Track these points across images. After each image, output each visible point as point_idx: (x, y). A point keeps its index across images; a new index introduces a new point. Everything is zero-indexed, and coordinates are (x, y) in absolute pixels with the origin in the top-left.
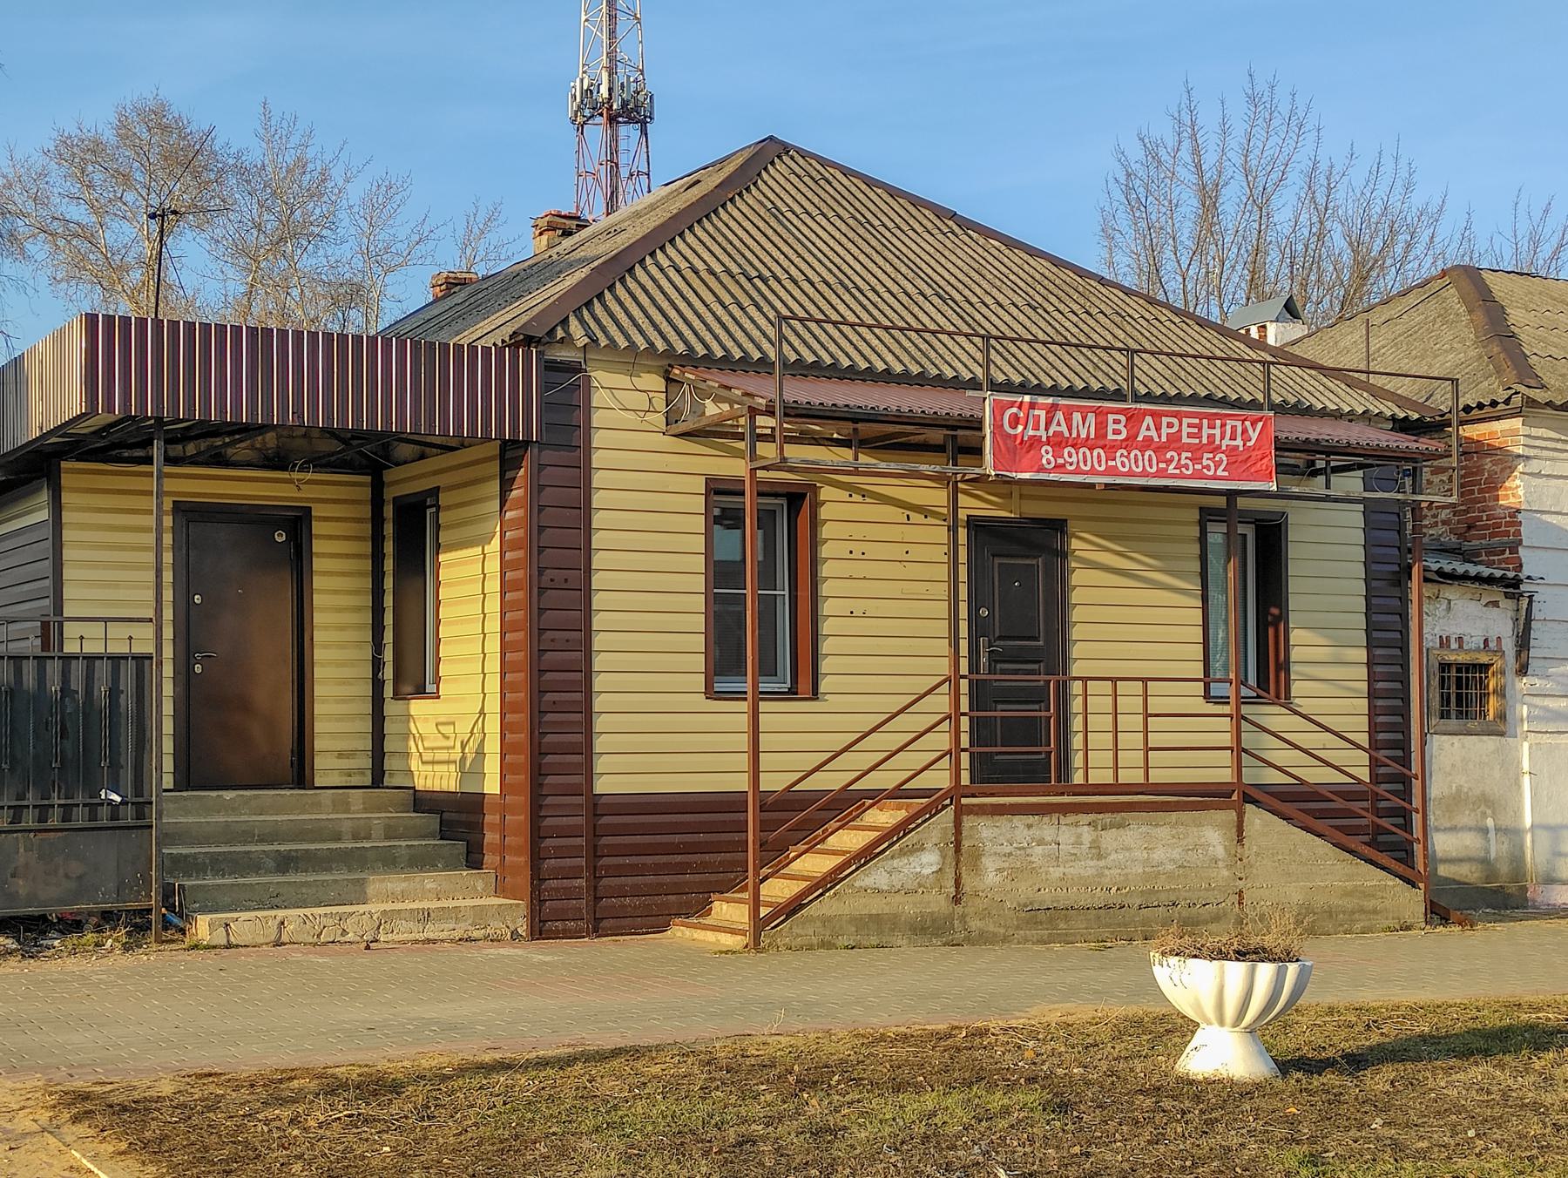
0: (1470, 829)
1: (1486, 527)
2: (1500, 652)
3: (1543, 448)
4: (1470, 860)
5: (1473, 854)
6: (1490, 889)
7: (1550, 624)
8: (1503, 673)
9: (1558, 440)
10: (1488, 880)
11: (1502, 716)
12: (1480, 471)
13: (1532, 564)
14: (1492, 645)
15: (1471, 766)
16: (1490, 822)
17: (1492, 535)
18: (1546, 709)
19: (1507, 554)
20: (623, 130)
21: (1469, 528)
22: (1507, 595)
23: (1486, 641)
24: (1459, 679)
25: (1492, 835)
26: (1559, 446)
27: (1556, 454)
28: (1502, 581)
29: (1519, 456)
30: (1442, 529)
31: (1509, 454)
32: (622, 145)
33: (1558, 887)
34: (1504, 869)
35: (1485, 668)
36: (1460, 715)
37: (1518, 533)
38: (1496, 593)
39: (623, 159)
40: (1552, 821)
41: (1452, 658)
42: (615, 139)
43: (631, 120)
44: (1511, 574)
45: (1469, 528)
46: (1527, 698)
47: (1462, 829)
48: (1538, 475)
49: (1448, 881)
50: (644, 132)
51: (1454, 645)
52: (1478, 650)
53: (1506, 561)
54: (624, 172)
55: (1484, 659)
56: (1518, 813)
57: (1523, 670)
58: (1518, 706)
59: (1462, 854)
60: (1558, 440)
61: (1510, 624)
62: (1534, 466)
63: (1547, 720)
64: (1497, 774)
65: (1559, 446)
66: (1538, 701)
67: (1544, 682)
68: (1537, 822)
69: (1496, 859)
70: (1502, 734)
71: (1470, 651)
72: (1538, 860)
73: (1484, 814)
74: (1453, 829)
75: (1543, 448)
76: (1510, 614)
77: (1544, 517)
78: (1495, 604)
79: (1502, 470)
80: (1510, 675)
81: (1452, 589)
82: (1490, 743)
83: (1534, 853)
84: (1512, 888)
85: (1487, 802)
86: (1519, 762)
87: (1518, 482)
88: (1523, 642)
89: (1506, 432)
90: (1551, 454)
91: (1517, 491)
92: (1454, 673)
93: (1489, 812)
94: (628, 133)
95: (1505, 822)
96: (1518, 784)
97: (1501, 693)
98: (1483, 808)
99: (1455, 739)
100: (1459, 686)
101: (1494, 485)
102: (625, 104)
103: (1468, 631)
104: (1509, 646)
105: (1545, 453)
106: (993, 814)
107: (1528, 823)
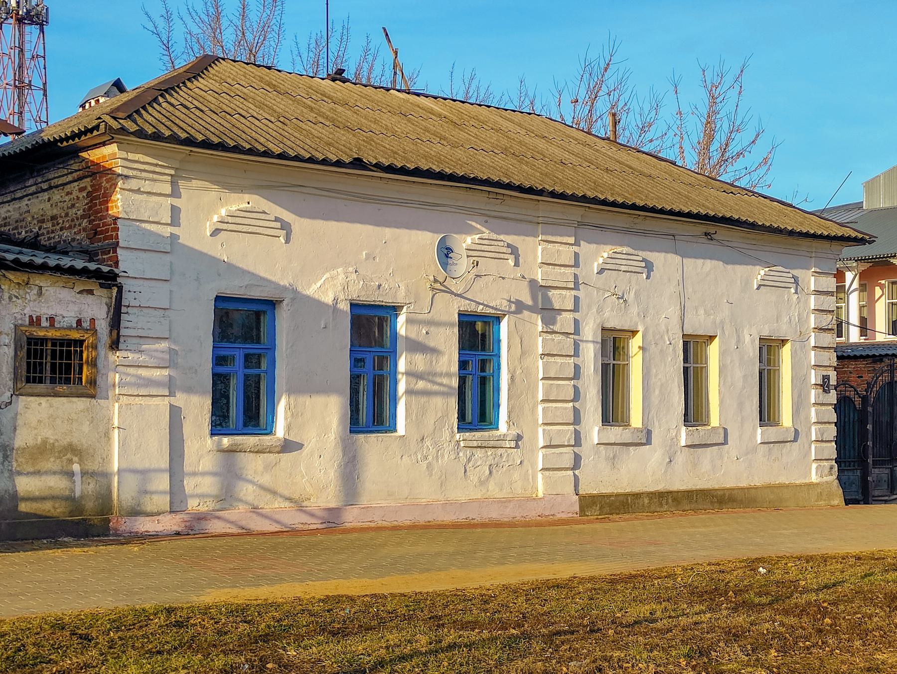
0: (55, 473)
1: (102, 232)
2: (93, 330)
3: (141, 170)
4: (53, 498)
5: (56, 493)
6: (72, 521)
7: (145, 310)
8: (95, 347)
9: (156, 165)
10: (71, 513)
11: (93, 382)
12: (100, 185)
13: (128, 263)
14: (86, 325)
15: (58, 421)
16: (76, 468)
17: (105, 239)
18: (139, 377)
19: (111, 254)
20: (28, 28)
21: (96, 234)
22: (102, 286)
23: (79, 322)
24: (54, 352)
25: (78, 478)
26: (158, 169)
27: (155, 176)
28: (97, 275)
29: (119, 175)
30: (83, 234)
31: (114, 173)
32: (27, 38)
33: (141, 519)
34: (90, 505)
35: (81, 342)
36: (53, 381)
37: (117, 237)
38: (93, 285)
39: (27, 47)
40: (139, 466)
41: (41, 334)
42: (22, 35)
43: (33, 23)
44: (106, 269)
45: (96, 234)
46: (117, 368)
47: (46, 473)
48: (138, 191)
49: (28, 515)
50: (42, 31)
51: (44, 323)
52: (70, 328)
53: (110, 259)
54: (28, 55)
55: (75, 335)
56: (107, 459)
57: (115, 345)
58: (111, 374)
59: (47, 493)
60: (156, 165)
61: (105, 308)
62: (133, 184)
63: (139, 386)
64: (86, 428)
65: (158, 169)
66: (131, 370)
67: (136, 356)
68: (124, 466)
69: (82, 497)
70: (93, 396)
71: (59, 329)
72: (123, 497)
73: (70, 461)
74: (38, 473)
75: (141, 170)
76: (104, 300)
77: (143, 225)
78: (90, 292)
79: (111, 186)
80: (103, 350)
81: (43, 278)
82: (80, 404)
83: (122, 492)
84: (96, 520)
85: (74, 450)
86: (110, 419)
87: (119, 196)
88: (115, 323)
89: (108, 154)
90: (151, 175)
91: (120, 203)
92: (49, 346)
93: (76, 459)
94: (31, 31)
95: (92, 466)
96: (107, 436)
97: (94, 364)
98: (69, 456)
99: (43, 400)
100: (53, 357)
101: (106, 198)
102: (28, 12)
103: (60, 312)
104: (103, 326)
105: (144, 175)
106: (637, 496)
107: (116, 469)
